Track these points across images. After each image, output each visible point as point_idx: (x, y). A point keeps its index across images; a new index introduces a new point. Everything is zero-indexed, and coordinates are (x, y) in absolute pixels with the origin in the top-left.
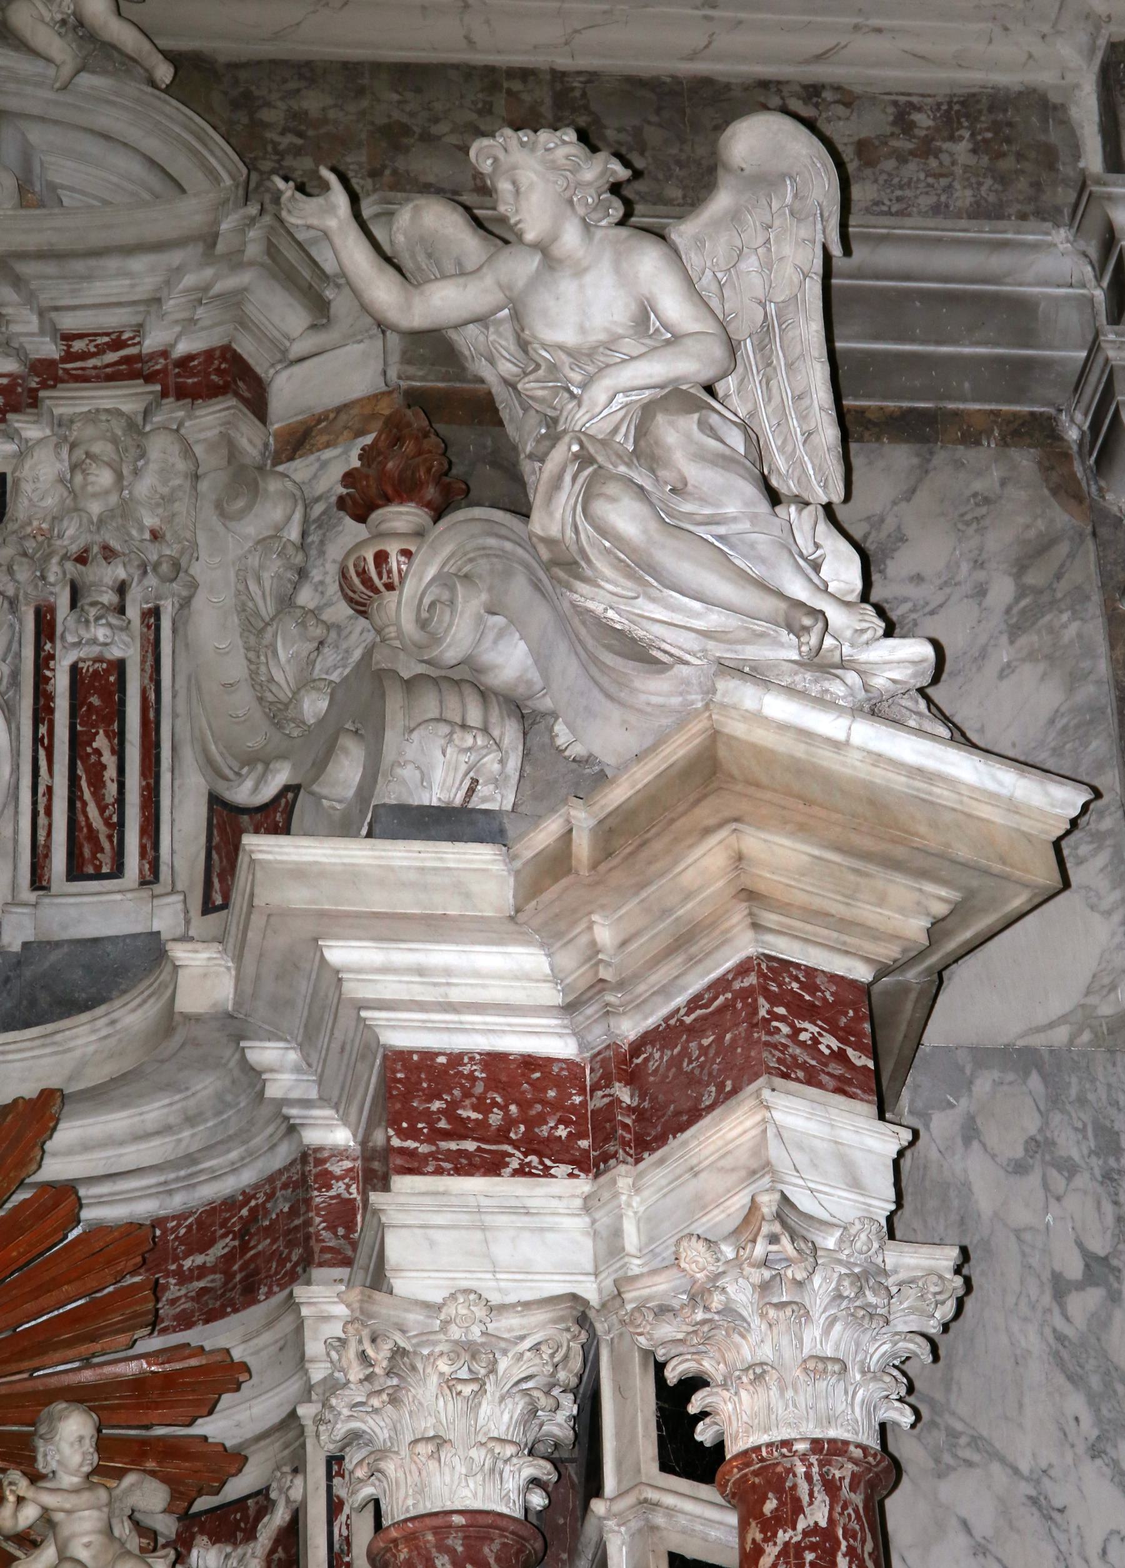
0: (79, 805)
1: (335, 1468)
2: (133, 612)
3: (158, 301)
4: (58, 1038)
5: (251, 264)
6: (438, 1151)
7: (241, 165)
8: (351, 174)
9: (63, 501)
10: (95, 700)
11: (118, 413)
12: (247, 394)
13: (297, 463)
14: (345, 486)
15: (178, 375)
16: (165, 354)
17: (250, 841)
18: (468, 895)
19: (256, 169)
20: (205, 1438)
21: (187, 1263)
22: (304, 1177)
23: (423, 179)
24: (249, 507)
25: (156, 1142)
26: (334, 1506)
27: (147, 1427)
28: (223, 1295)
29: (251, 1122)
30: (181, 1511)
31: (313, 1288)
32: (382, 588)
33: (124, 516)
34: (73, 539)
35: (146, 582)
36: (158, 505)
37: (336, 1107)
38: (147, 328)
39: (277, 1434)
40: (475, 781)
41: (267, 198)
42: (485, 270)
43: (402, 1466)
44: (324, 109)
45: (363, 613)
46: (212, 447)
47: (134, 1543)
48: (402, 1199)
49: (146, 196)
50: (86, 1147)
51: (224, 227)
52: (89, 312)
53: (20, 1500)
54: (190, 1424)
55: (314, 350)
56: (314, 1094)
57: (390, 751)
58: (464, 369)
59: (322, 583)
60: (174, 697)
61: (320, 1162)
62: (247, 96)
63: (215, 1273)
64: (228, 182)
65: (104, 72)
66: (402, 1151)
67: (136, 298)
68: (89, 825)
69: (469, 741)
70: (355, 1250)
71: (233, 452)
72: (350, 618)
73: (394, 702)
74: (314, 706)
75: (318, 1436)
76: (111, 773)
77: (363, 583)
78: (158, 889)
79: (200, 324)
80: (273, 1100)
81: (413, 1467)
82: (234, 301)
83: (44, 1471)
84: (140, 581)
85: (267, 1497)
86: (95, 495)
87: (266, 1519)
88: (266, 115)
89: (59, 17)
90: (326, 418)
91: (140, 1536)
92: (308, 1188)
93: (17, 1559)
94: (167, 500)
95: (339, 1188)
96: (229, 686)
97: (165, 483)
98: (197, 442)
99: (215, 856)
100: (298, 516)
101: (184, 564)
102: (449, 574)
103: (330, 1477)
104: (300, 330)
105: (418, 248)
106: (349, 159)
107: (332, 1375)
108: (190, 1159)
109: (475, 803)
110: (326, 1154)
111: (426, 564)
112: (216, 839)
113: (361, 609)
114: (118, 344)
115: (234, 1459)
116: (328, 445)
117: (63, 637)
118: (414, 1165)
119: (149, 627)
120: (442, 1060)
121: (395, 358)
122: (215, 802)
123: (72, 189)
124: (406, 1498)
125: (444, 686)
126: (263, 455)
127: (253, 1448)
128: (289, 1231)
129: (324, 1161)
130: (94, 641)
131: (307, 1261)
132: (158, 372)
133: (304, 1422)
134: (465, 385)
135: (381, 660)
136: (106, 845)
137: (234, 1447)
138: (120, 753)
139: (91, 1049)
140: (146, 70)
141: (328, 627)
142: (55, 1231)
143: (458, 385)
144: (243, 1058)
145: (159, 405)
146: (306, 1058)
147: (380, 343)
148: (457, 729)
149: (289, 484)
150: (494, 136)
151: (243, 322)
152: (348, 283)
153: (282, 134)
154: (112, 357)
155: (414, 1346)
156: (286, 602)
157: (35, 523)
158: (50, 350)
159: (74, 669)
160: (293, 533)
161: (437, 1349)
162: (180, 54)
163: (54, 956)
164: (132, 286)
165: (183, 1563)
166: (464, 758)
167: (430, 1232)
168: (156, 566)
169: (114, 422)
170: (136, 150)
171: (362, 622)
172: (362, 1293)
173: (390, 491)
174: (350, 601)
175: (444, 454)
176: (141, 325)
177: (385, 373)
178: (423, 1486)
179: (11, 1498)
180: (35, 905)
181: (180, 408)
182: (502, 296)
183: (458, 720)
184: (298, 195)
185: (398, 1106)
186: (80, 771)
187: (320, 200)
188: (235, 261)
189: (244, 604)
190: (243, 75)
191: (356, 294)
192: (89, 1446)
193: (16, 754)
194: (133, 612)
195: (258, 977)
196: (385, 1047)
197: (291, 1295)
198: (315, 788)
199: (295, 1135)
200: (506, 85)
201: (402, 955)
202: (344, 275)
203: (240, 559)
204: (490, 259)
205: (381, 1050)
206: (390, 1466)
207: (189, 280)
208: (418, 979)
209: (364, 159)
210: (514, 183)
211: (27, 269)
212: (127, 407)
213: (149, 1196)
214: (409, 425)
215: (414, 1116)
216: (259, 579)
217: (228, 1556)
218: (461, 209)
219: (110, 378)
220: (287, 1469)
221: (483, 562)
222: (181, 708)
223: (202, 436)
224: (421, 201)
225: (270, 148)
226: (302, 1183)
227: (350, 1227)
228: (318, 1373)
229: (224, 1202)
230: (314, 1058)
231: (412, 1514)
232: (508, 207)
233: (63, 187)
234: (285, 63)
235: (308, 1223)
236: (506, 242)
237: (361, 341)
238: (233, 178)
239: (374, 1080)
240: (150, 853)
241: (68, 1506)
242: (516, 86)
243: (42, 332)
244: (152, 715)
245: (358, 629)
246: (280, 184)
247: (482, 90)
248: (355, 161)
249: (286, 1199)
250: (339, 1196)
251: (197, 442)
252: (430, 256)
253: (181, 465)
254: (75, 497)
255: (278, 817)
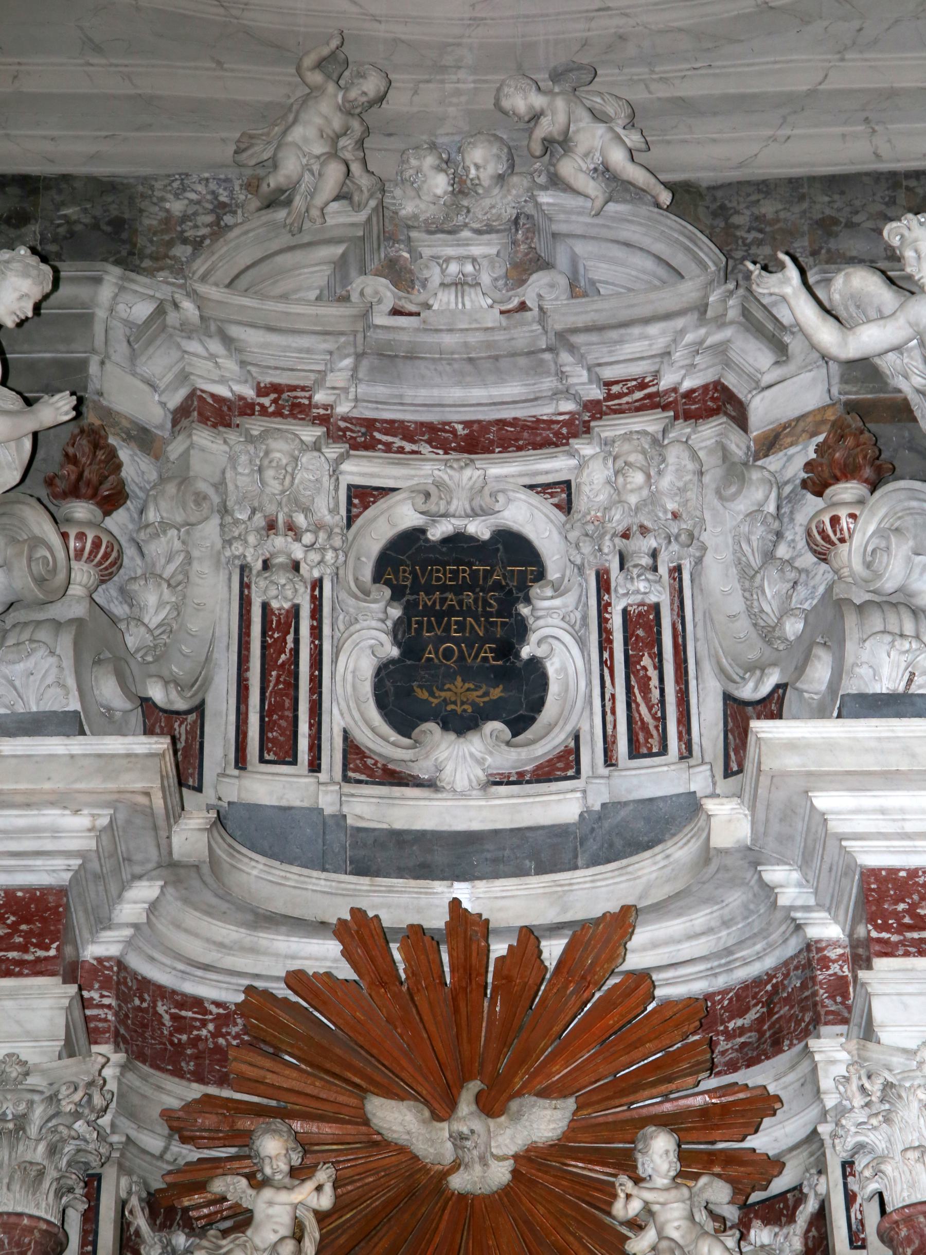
0: (634, 706)
1: (848, 1170)
2: (663, 570)
3: (669, 353)
4: (630, 869)
5: (732, 323)
6: (905, 939)
7: (721, 256)
8: (798, 255)
9: (611, 496)
10: (640, 632)
11: (645, 433)
12: (733, 414)
13: (771, 458)
14: (806, 472)
15: (685, 404)
16: (675, 390)
17: (756, 725)
18: (913, 756)
19: (732, 258)
20: (754, 1150)
21: (731, 1025)
22: (809, 961)
23: (849, 254)
24: (739, 492)
25: (703, 940)
26: (850, 1198)
27: (713, 1143)
28: (757, 1047)
29: (769, 924)
30: (741, 1203)
31: (822, 1040)
32: (837, 542)
33: (652, 503)
34: (619, 522)
35: (671, 548)
36: (676, 494)
37: (829, 910)
38: (662, 373)
39: (805, 1146)
40: (912, 674)
41: (740, 276)
42: (898, 313)
43: (897, 1168)
44: (777, 212)
45: (825, 560)
46: (711, 451)
47: (710, 1226)
48: (881, 975)
49: (657, 283)
50: (655, 945)
51: (711, 299)
52: (621, 366)
53: (628, 1196)
54: (743, 1140)
55: (779, 379)
56: (812, 902)
57: (849, 658)
58: (886, 384)
59: (793, 541)
60: (695, 627)
61: (819, 950)
62: (723, 207)
63: (751, 1031)
64: (713, 268)
65: (625, 201)
66: (879, 941)
67: (653, 353)
68: (642, 720)
69: (907, 646)
70: (850, 1012)
71: (725, 455)
72: (815, 564)
73: (851, 621)
74: (793, 627)
75: (834, 1146)
76: (654, 682)
77: (823, 539)
78: (692, 762)
79: (698, 368)
80: (784, 907)
81: (906, 1168)
82: (721, 351)
83: (643, 1176)
84: (667, 548)
85: (801, 1191)
86: (632, 491)
87: (801, 1208)
88: (736, 220)
89: (592, 166)
90: (790, 425)
91: (714, 1221)
92: (813, 970)
93: (629, 1238)
94: (682, 490)
95: (835, 968)
96: (732, 617)
97: (680, 478)
98: (700, 449)
99: (730, 736)
100: (773, 495)
101: (696, 534)
102: (884, 529)
103: (845, 1176)
104: (768, 366)
105: (850, 302)
106: (795, 245)
107: (840, 1102)
108: (728, 951)
109: (913, 689)
110: (824, 944)
111: (867, 523)
112: (731, 725)
113: (823, 557)
114: (642, 386)
115: (775, 1165)
116: (791, 445)
117: (616, 591)
118: (888, 950)
119: (674, 579)
120: (903, 874)
121: (836, 380)
122: (728, 699)
123: (607, 283)
124: (902, 1190)
125: (886, 607)
126: (747, 454)
127: (788, 1156)
128: (802, 1000)
129: (823, 949)
130: (638, 592)
131: (816, 1021)
132: (671, 403)
133: (823, 1137)
134: (886, 395)
135: (840, 592)
136: (654, 733)
137: (774, 1156)
138: (660, 668)
139: (654, 875)
140: (653, 197)
141: (800, 571)
142: (638, 1005)
143: (882, 395)
144: (760, 879)
145: (673, 426)
146: (805, 876)
147: (825, 371)
148: (897, 638)
149: (766, 473)
150: (900, 220)
151: (728, 363)
152: (801, 330)
153: (749, 231)
154: (639, 395)
155: (899, 1080)
156: (769, 556)
157: (593, 513)
158: (596, 393)
159: (625, 612)
160: (771, 508)
161: (916, 1083)
162: (675, 184)
163: (623, 813)
164: (650, 345)
165: (745, 1240)
166: (904, 658)
167: (905, 998)
168: (677, 537)
169: (643, 440)
170: (648, 252)
171: (824, 566)
172: (858, 1043)
173: (838, 474)
174: (815, 552)
175: (875, 444)
176: (658, 371)
177: (829, 391)
178: (914, 1183)
179: (622, 1195)
180: (608, 777)
181: (688, 426)
182: (911, 330)
183: (897, 631)
184: (763, 273)
185: (874, 908)
186: (633, 682)
187: (779, 275)
188: (720, 322)
189: (739, 559)
190: (719, 194)
191: (807, 337)
192: (673, 1157)
193: (589, 672)
194: (663, 570)
195: (767, 820)
196: (861, 866)
197: (806, 1046)
198: (798, 685)
199: (801, 931)
200: (904, 183)
201: (867, 800)
202: (798, 324)
203: (735, 528)
204: (901, 305)
205: (858, 870)
206: (888, 1168)
207: (689, 338)
208: (881, 817)
209: (806, 244)
210: (916, 251)
211: (578, 339)
212: (651, 429)
213: (701, 978)
214: (849, 426)
215: (885, 915)
216: (749, 541)
217: (776, 1235)
218: (879, 273)
219: (638, 409)
220: (813, 1171)
221: (908, 518)
222: (700, 634)
223: (703, 444)
224: (850, 270)
225: (740, 242)
226: (809, 965)
227: (845, 996)
228: (830, 1101)
229: (754, 981)
230: (810, 878)
231: (908, 1202)
232: (914, 269)
233: (600, 282)
234: (748, 183)
235: (815, 994)
236: (913, 293)
237: (810, 371)
238: (716, 264)
239: (854, 891)
240: (685, 737)
241: (661, 1200)
242: (913, 183)
243: (590, 381)
244: (680, 640)
245: (821, 572)
246: (751, 267)
247: (888, 189)
248: (801, 246)
249: (798, 978)
250: (835, 974)
251: (700, 449)
252: (858, 307)
253: (691, 466)
254: (619, 493)
255: (773, 707)
